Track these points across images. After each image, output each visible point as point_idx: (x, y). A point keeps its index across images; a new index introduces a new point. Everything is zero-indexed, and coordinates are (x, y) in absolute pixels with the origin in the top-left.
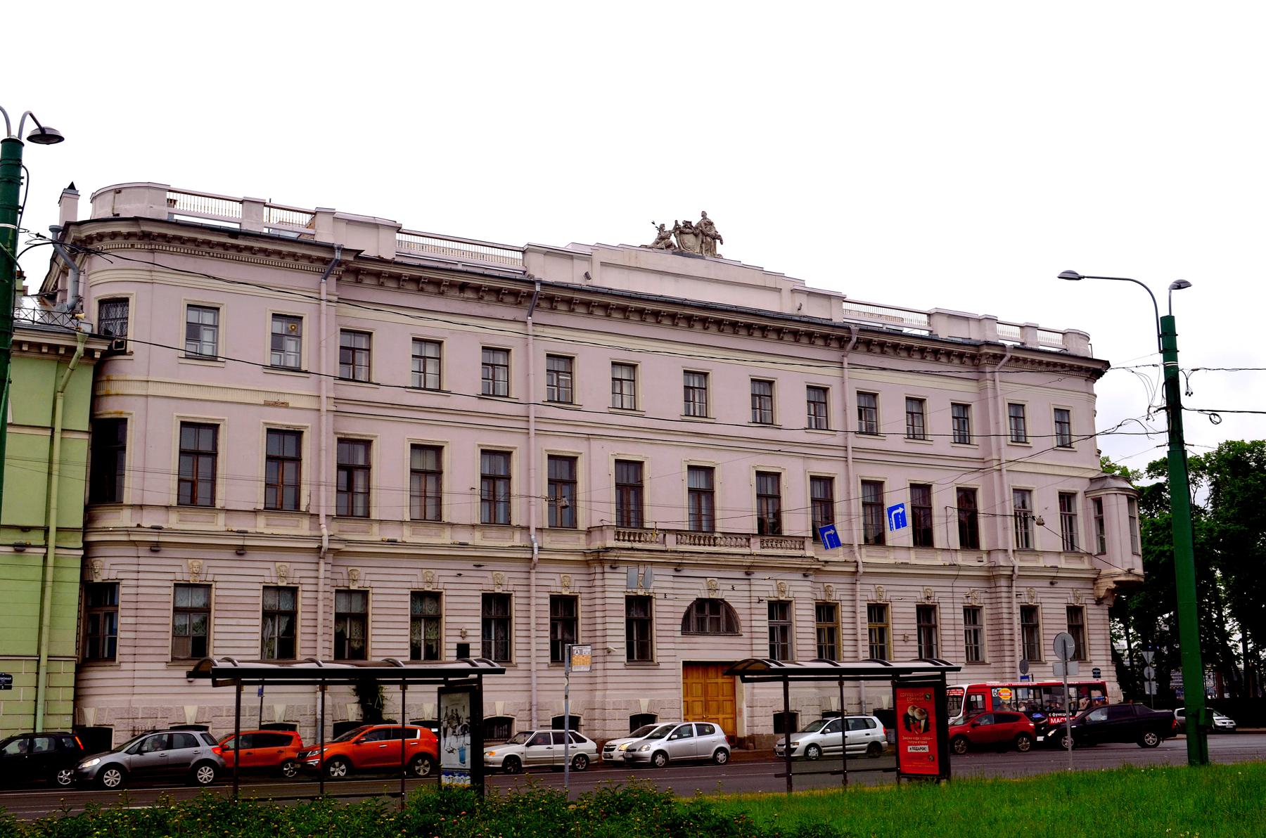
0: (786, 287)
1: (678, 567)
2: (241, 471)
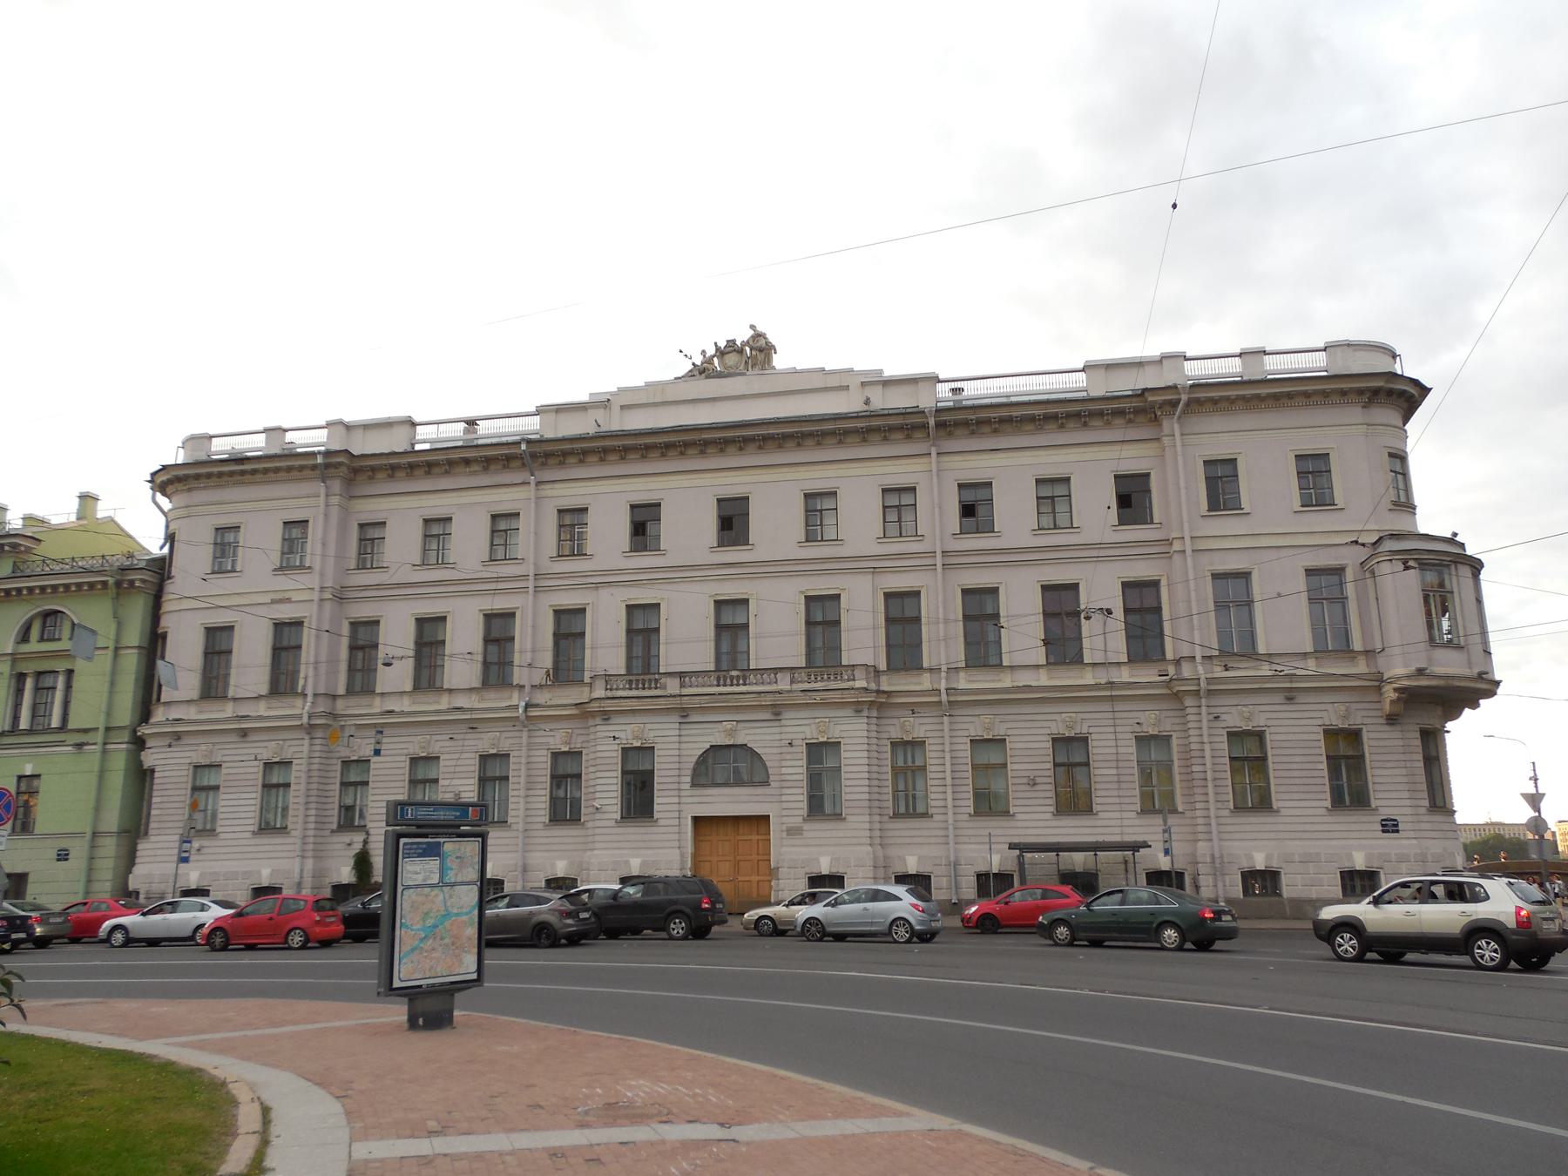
0: (854, 383)
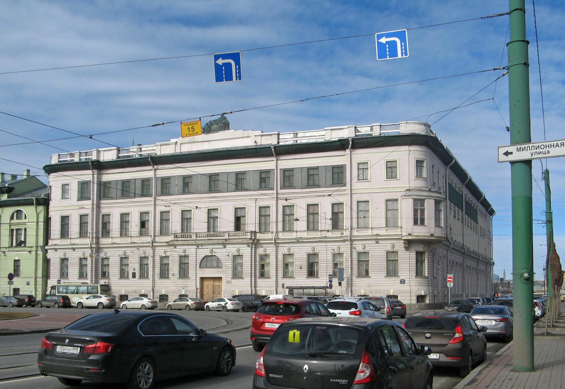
2: (74, 227)
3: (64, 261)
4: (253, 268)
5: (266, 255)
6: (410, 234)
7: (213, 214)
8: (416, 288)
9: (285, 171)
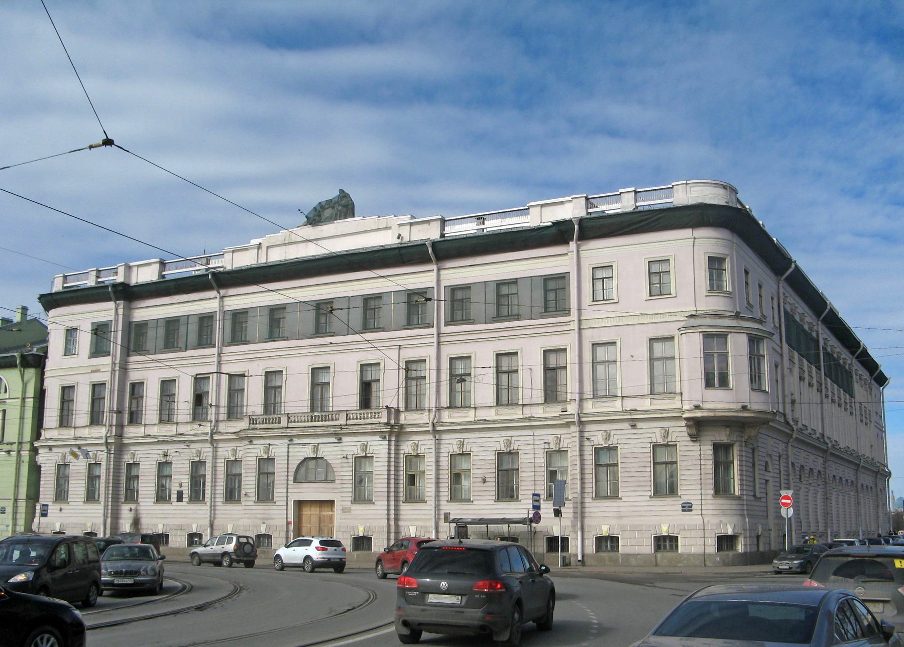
1: (291, 438)
3: (62, 469)
4: (392, 481)
5: (417, 456)
6: (697, 407)
7: (323, 378)
8: (715, 521)
9: (454, 289)
